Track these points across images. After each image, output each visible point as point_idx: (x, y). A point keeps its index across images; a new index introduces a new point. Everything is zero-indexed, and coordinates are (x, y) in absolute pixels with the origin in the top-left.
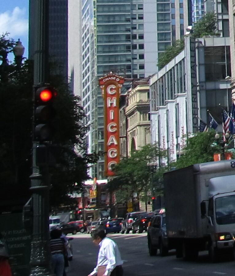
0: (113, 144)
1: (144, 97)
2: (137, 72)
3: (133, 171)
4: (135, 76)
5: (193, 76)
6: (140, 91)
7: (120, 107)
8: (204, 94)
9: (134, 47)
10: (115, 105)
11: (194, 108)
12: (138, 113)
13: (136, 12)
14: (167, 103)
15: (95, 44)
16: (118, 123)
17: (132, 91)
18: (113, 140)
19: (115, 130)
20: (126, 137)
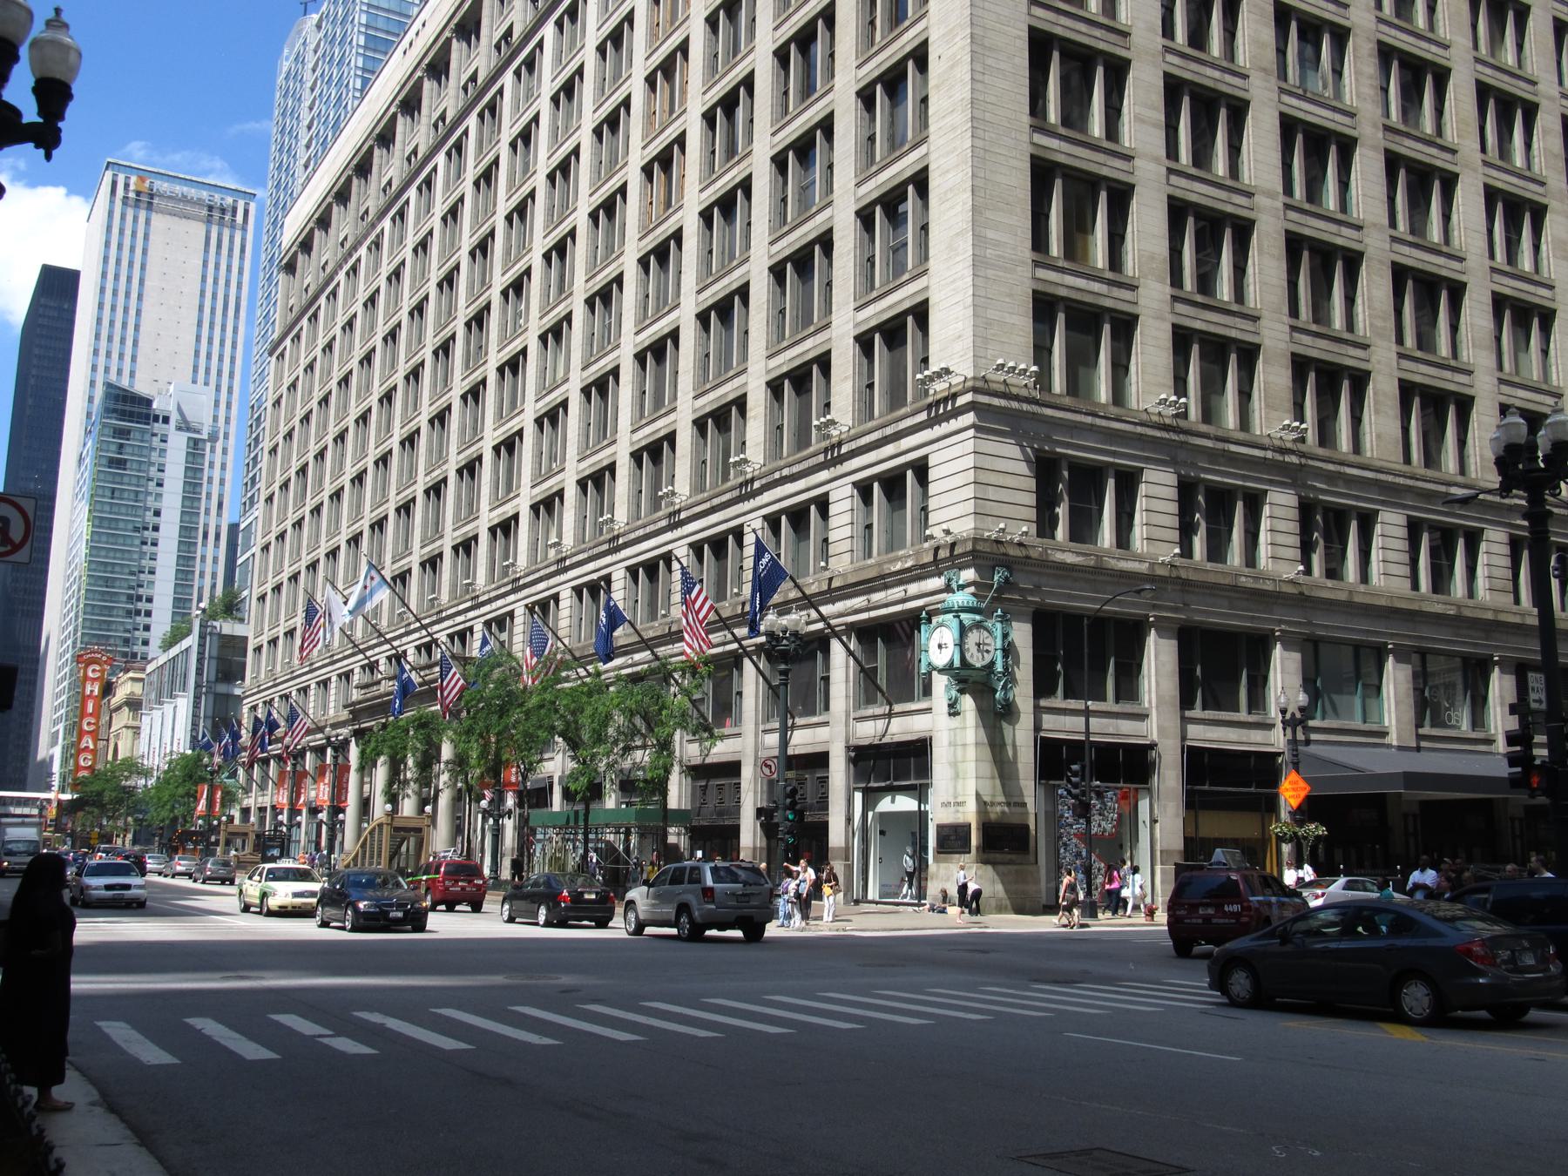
0: (87, 747)
1: (137, 689)
2: (139, 649)
3: (104, 791)
4: (134, 655)
5: (199, 672)
6: (133, 679)
8: (211, 698)
9: (138, 613)
10: (96, 693)
11: (195, 716)
12: (126, 709)
13: (146, 563)
14: (176, 696)
15: (84, 586)
16: (98, 718)
17: (124, 677)
18: (88, 742)
19: (92, 728)
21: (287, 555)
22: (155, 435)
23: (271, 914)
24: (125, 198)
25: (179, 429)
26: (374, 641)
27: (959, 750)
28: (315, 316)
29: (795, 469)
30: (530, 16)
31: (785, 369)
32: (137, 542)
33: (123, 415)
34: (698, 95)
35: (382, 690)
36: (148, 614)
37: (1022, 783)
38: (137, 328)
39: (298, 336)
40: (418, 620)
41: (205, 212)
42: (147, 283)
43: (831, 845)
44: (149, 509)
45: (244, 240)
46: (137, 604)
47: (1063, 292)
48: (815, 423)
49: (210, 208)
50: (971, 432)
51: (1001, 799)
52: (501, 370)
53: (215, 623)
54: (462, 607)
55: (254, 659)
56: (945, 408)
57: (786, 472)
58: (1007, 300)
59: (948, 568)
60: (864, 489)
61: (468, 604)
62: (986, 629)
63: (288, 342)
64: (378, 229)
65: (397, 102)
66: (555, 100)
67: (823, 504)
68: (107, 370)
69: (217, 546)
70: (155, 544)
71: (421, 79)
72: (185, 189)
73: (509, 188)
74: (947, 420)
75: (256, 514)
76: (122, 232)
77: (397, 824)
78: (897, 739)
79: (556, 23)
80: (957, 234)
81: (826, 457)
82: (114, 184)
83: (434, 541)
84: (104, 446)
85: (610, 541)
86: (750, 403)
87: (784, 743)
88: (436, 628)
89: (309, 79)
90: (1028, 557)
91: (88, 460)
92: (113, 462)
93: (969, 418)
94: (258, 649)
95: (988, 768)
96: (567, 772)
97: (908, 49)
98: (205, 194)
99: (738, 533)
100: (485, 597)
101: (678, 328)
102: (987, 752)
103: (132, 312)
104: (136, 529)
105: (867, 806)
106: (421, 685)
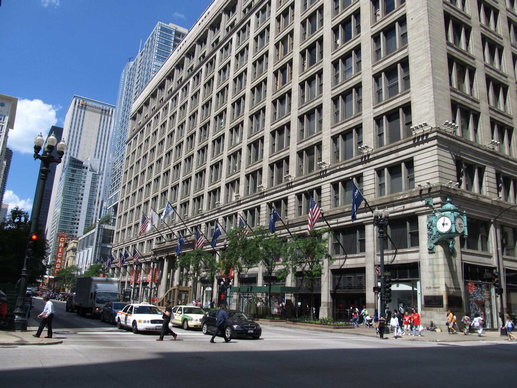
1: (75, 245)
2: (74, 234)
4: (73, 236)
5: (97, 240)
6: (74, 242)
7: (64, 247)
8: (100, 248)
9: (75, 223)
10: (62, 246)
11: (95, 253)
12: (72, 251)
13: (78, 209)
14: (84, 249)
16: (62, 254)
18: (59, 261)
19: (61, 256)
20: (65, 260)
21: (130, 203)
22: (83, 172)
23: (189, 329)
24: (79, 106)
25: (90, 171)
26: (181, 223)
27: (435, 268)
28: (143, 131)
29: (346, 165)
30: (211, 49)
31: (340, 131)
32: (76, 203)
33: (74, 166)
34: (230, 99)
35: (166, 245)
36: (78, 224)
37: (459, 280)
38: (79, 142)
39: (136, 138)
40: (168, 226)
41: (101, 111)
42: (83, 130)
43: (367, 302)
44: (80, 193)
45: (111, 119)
46: (75, 221)
47: (459, 101)
48: (258, 186)
49: (102, 110)
50: (436, 147)
51: (453, 286)
52: (214, 142)
53: (103, 225)
54: (151, 234)
55: (116, 236)
56: (323, 174)
57: (342, 167)
58: (444, 101)
59: (426, 198)
60: (379, 172)
61: (200, 217)
62: (461, 218)
63: (133, 140)
64: (167, 103)
65: (175, 65)
66: (192, 98)
67: (259, 208)
68: (70, 154)
69: (98, 206)
70: (81, 204)
71: (184, 58)
72: (96, 104)
73: (218, 85)
74: (423, 143)
75: (119, 190)
76: (77, 115)
77: (180, 289)
78: (399, 262)
79: (256, 14)
80: (425, 78)
81: (320, 174)
82: (76, 102)
83: (186, 197)
84: (68, 175)
85: (187, 220)
86: (324, 144)
87: (382, 259)
88: (162, 232)
89: (138, 69)
90: (457, 194)
91: (63, 179)
92: (71, 180)
93: (435, 142)
94: (118, 233)
95: (448, 274)
96: (264, 272)
97: (396, 18)
98: (101, 106)
99: (236, 214)
100: (207, 214)
101: (290, 121)
102: (448, 267)
103: (78, 138)
104: (76, 199)
105: (204, 290)
106: (186, 242)
